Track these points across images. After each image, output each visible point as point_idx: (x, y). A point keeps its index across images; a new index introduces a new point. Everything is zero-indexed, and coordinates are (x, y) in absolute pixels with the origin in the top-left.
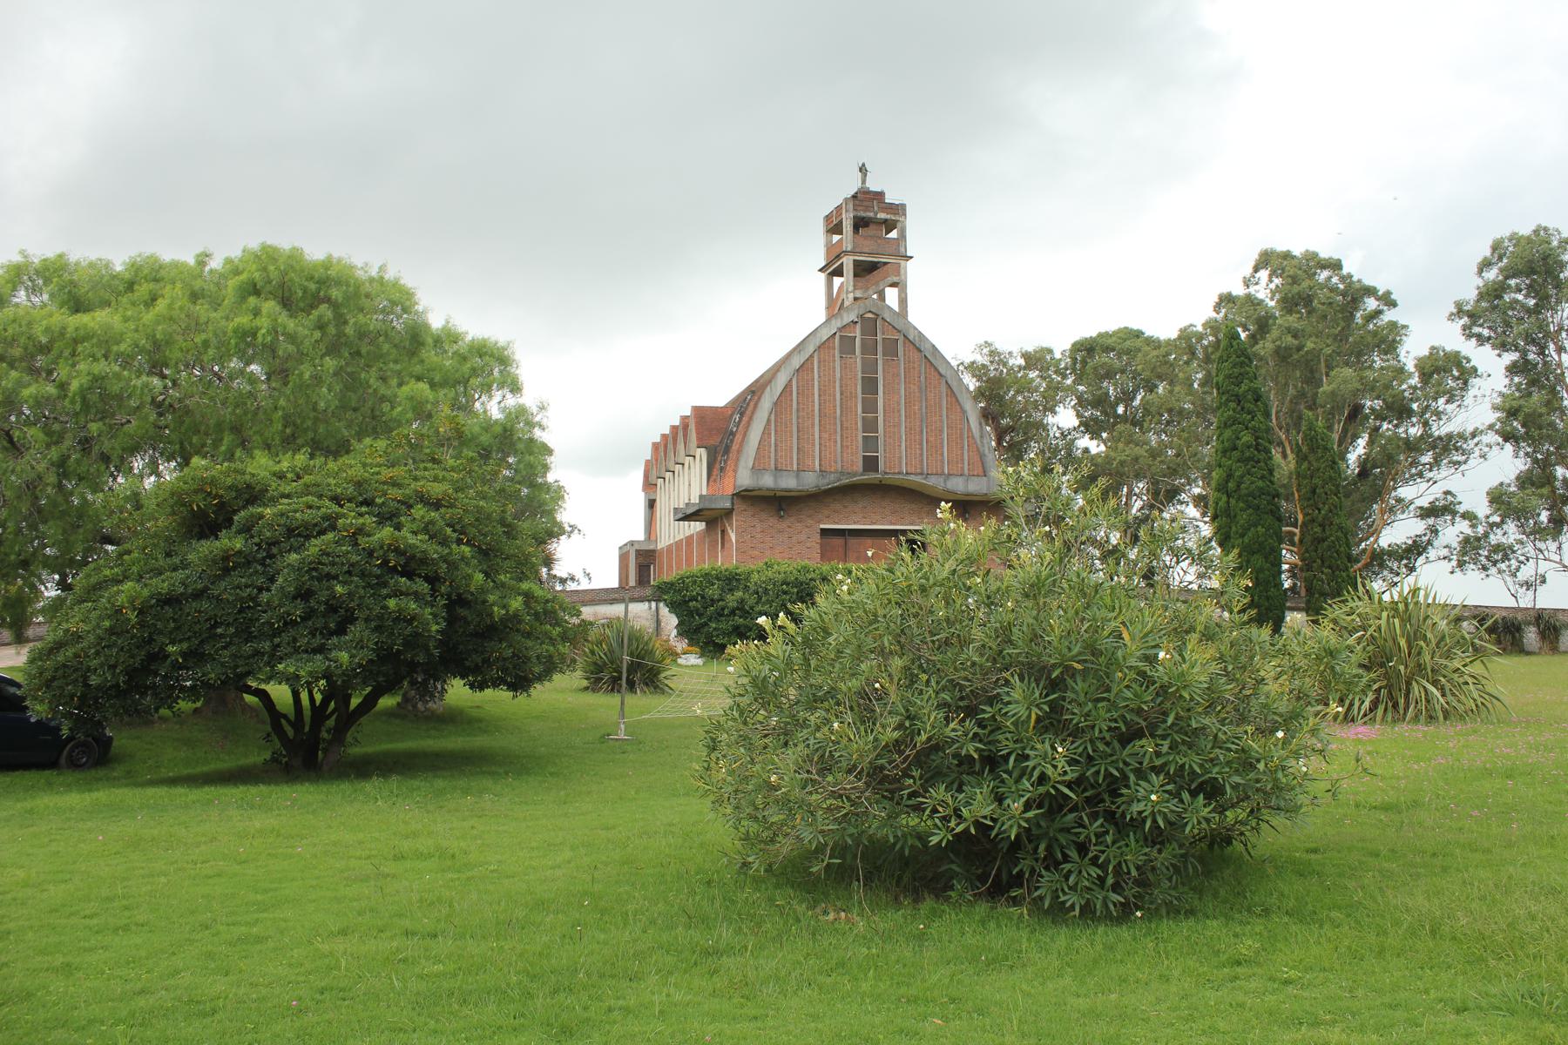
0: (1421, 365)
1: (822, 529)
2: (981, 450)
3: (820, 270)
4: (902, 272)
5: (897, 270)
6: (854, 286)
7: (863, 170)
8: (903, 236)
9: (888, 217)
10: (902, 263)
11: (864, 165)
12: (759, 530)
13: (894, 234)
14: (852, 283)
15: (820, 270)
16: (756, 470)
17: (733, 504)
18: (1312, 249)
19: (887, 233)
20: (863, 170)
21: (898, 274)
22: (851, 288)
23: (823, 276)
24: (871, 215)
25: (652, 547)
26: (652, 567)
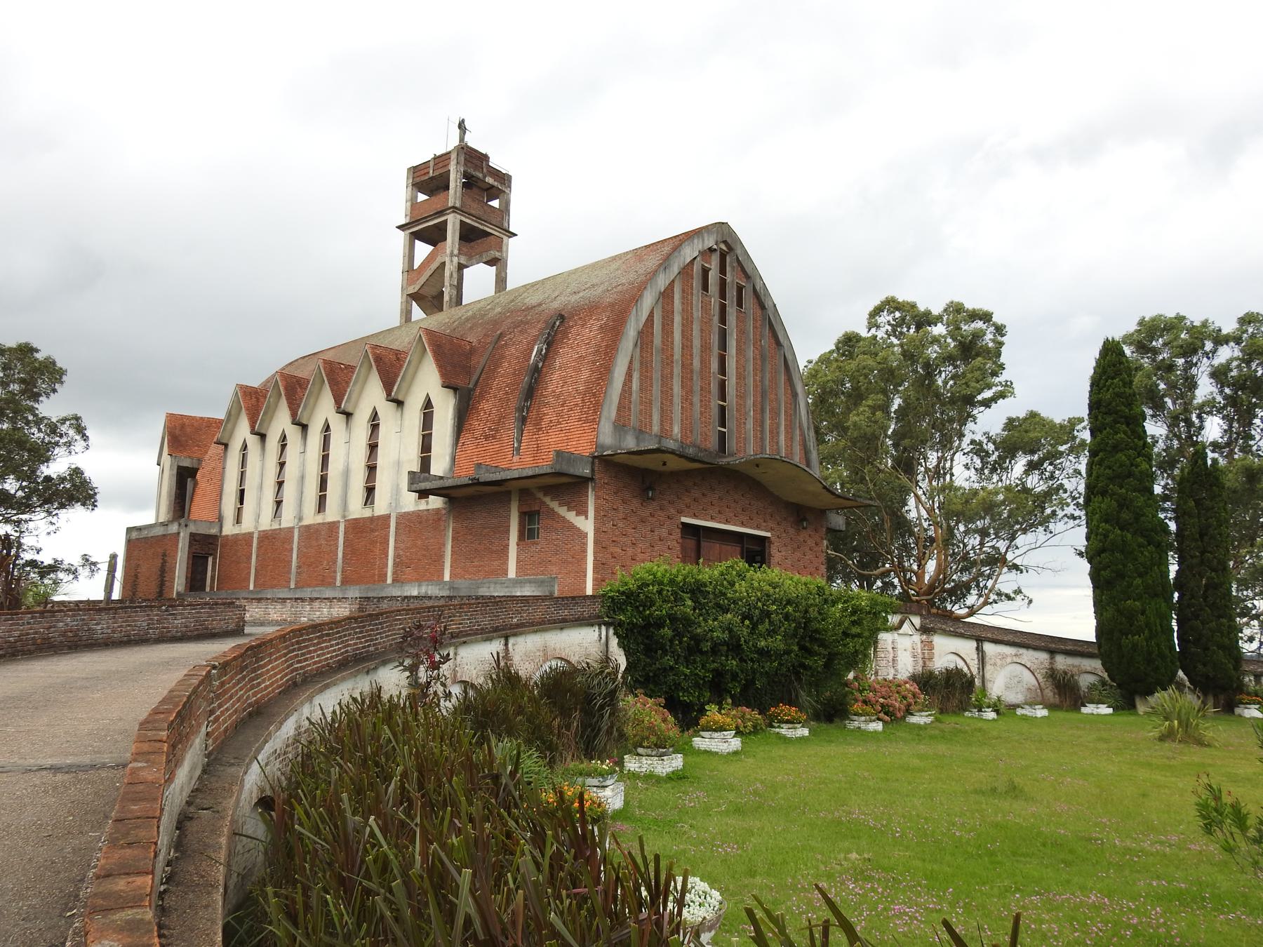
0: (46, 477)
1: (682, 523)
2: (808, 443)
3: (399, 227)
4: (504, 249)
5: (500, 246)
6: (459, 250)
7: (462, 126)
8: (505, 209)
9: (496, 184)
10: (505, 238)
11: (463, 121)
12: (621, 515)
13: (495, 203)
14: (457, 246)
15: (399, 227)
16: (620, 426)
17: (593, 470)
18: (956, 300)
19: (490, 200)
20: (462, 126)
21: (500, 249)
22: (456, 252)
23: (401, 237)
24: (480, 175)
25: (214, 531)
26: (210, 560)
